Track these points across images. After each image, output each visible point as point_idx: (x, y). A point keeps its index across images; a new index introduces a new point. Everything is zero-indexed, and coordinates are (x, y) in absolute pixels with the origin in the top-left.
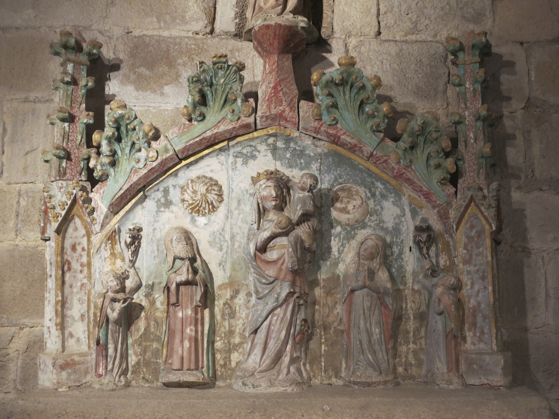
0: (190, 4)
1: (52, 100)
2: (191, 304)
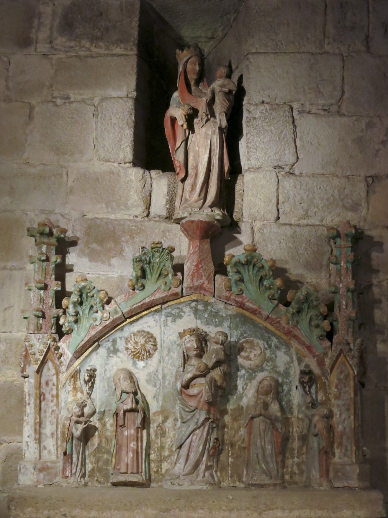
0: (131, 194)
1: (25, 268)
2: (134, 425)
